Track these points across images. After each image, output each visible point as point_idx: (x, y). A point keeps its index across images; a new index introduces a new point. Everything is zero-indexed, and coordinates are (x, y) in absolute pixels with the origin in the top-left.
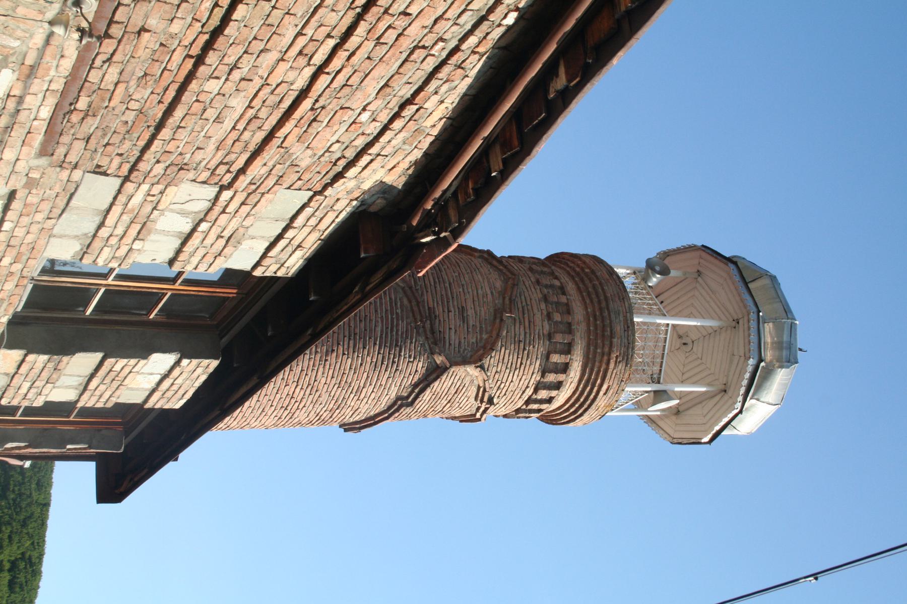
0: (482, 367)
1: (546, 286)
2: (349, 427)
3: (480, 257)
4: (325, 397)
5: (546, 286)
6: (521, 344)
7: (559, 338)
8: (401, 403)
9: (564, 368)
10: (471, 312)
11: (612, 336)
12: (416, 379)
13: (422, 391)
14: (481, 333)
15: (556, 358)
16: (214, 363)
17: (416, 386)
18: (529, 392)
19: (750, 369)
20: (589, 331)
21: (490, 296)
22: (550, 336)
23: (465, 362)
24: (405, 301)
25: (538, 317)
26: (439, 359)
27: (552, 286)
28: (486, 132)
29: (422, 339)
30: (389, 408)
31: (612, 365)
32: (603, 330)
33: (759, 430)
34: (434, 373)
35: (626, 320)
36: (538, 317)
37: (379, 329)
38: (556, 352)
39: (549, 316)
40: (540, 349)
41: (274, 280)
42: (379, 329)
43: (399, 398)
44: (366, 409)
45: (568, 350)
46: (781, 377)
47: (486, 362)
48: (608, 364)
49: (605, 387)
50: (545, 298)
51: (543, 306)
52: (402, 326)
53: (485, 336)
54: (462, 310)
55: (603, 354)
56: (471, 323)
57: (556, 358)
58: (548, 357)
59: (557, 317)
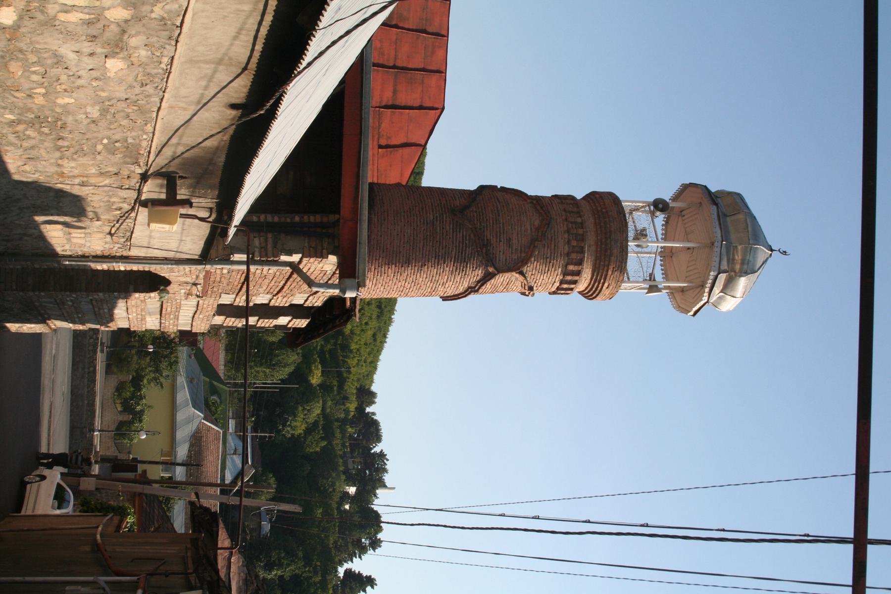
0: (522, 273)
1: (572, 223)
2: (445, 299)
3: (532, 203)
4: (424, 287)
5: (572, 223)
6: (548, 260)
7: (574, 256)
8: (472, 290)
9: (578, 273)
10: (515, 241)
11: (611, 255)
12: (479, 278)
13: (482, 285)
14: (521, 252)
15: (571, 268)
16: (308, 321)
17: (478, 282)
18: (557, 284)
19: (711, 277)
20: (597, 251)
21: (529, 231)
22: (568, 254)
23: (509, 270)
24: (472, 236)
25: (562, 242)
26: (491, 270)
27: (575, 222)
28: (28, 579)
29: (480, 258)
30: (466, 291)
31: (610, 272)
32: (606, 251)
33: (735, 309)
34: (487, 278)
35: (621, 247)
36: (562, 242)
37: (454, 253)
38: (572, 264)
39: (569, 242)
40: (562, 261)
41: (313, 307)
42: (454, 253)
43: (469, 287)
44: (450, 293)
45: (580, 263)
46: (742, 282)
47: (525, 269)
48: (607, 271)
49: (606, 285)
50: (568, 231)
51: (566, 236)
52: (469, 250)
53: (523, 255)
54: (509, 240)
55: (604, 266)
56: (514, 247)
57: (571, 268)
58: (566, 266)
59: (574, 243)
